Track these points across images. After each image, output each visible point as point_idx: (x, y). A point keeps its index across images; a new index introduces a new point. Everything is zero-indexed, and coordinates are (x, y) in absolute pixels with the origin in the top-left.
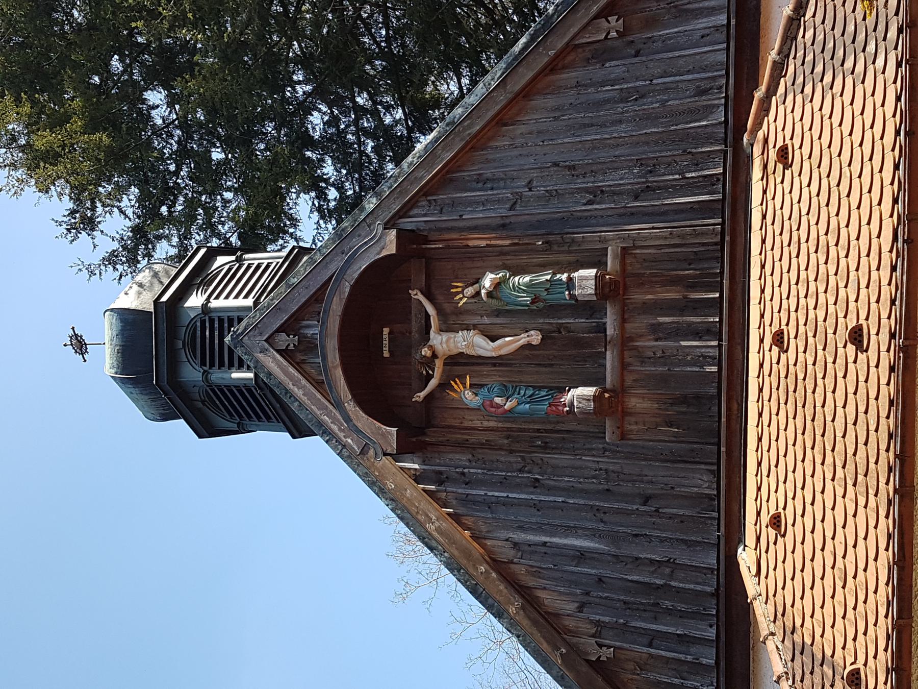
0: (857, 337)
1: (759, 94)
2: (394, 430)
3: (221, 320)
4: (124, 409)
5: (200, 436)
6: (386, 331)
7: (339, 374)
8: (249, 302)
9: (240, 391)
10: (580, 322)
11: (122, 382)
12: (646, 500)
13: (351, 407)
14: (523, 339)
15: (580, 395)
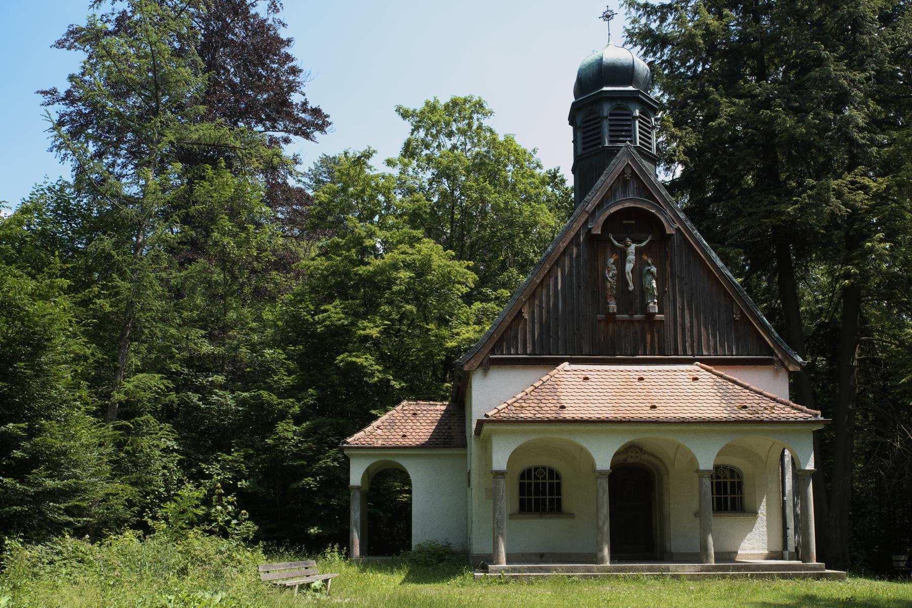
0: (653, 407)
1: (805, 408)
3: (630, 131)
9: (599, 133)
10: (638, 304)
12: (578, 330)
14: (631, 284)
15: (613, 306)
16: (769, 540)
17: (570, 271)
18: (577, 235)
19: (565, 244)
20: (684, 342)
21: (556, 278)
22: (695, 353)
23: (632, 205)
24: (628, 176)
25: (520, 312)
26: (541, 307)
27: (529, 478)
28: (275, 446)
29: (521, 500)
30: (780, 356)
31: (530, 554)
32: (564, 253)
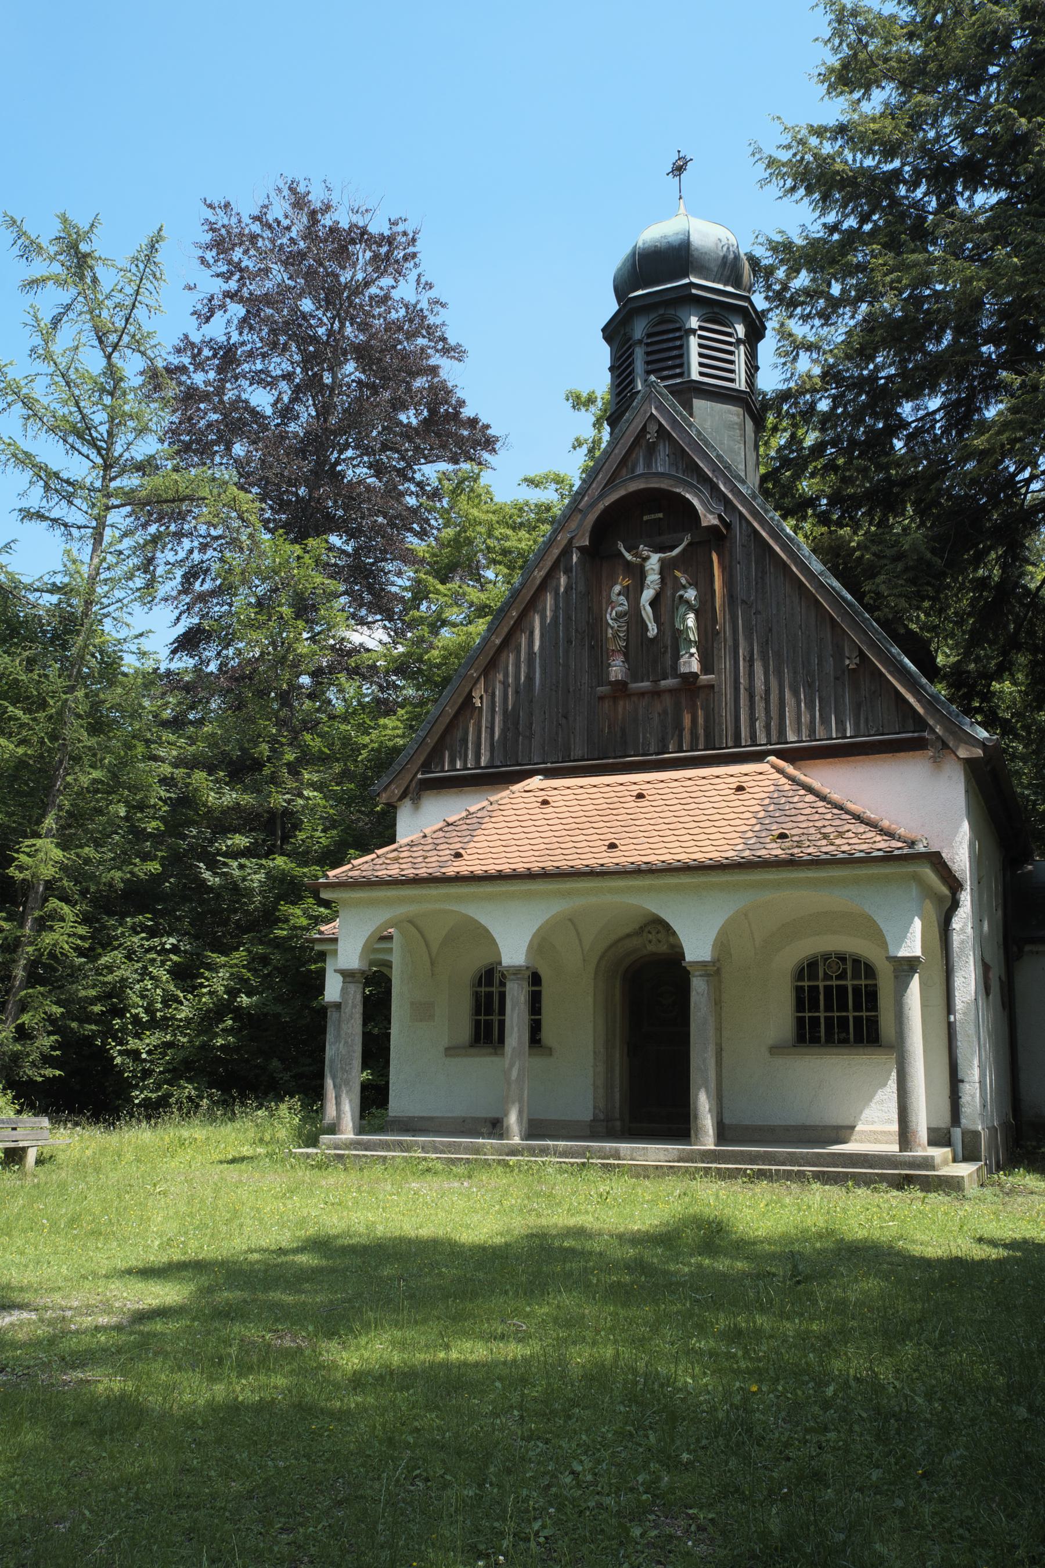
3: (681, 356)
5: (603, 330)
6: (661, 515)
7: (622, 492)
8: (695, 376)
11: (633, 253)
13: (601, 506)
15: (617, 669)
17: (555, 618)
18: (566, 552)
19: (543, 573)
20: (752, 720)
21: (532, 633)
22: (774, 739)
23: (642, 486)
24: (652, 437)
25: (469, 697)
26: (505, 685)
27: (813, 976)
28: (289, 938)
29: (477, 1023)
30: (938, 729)
31: (476, 1120)
32: (543, 587)
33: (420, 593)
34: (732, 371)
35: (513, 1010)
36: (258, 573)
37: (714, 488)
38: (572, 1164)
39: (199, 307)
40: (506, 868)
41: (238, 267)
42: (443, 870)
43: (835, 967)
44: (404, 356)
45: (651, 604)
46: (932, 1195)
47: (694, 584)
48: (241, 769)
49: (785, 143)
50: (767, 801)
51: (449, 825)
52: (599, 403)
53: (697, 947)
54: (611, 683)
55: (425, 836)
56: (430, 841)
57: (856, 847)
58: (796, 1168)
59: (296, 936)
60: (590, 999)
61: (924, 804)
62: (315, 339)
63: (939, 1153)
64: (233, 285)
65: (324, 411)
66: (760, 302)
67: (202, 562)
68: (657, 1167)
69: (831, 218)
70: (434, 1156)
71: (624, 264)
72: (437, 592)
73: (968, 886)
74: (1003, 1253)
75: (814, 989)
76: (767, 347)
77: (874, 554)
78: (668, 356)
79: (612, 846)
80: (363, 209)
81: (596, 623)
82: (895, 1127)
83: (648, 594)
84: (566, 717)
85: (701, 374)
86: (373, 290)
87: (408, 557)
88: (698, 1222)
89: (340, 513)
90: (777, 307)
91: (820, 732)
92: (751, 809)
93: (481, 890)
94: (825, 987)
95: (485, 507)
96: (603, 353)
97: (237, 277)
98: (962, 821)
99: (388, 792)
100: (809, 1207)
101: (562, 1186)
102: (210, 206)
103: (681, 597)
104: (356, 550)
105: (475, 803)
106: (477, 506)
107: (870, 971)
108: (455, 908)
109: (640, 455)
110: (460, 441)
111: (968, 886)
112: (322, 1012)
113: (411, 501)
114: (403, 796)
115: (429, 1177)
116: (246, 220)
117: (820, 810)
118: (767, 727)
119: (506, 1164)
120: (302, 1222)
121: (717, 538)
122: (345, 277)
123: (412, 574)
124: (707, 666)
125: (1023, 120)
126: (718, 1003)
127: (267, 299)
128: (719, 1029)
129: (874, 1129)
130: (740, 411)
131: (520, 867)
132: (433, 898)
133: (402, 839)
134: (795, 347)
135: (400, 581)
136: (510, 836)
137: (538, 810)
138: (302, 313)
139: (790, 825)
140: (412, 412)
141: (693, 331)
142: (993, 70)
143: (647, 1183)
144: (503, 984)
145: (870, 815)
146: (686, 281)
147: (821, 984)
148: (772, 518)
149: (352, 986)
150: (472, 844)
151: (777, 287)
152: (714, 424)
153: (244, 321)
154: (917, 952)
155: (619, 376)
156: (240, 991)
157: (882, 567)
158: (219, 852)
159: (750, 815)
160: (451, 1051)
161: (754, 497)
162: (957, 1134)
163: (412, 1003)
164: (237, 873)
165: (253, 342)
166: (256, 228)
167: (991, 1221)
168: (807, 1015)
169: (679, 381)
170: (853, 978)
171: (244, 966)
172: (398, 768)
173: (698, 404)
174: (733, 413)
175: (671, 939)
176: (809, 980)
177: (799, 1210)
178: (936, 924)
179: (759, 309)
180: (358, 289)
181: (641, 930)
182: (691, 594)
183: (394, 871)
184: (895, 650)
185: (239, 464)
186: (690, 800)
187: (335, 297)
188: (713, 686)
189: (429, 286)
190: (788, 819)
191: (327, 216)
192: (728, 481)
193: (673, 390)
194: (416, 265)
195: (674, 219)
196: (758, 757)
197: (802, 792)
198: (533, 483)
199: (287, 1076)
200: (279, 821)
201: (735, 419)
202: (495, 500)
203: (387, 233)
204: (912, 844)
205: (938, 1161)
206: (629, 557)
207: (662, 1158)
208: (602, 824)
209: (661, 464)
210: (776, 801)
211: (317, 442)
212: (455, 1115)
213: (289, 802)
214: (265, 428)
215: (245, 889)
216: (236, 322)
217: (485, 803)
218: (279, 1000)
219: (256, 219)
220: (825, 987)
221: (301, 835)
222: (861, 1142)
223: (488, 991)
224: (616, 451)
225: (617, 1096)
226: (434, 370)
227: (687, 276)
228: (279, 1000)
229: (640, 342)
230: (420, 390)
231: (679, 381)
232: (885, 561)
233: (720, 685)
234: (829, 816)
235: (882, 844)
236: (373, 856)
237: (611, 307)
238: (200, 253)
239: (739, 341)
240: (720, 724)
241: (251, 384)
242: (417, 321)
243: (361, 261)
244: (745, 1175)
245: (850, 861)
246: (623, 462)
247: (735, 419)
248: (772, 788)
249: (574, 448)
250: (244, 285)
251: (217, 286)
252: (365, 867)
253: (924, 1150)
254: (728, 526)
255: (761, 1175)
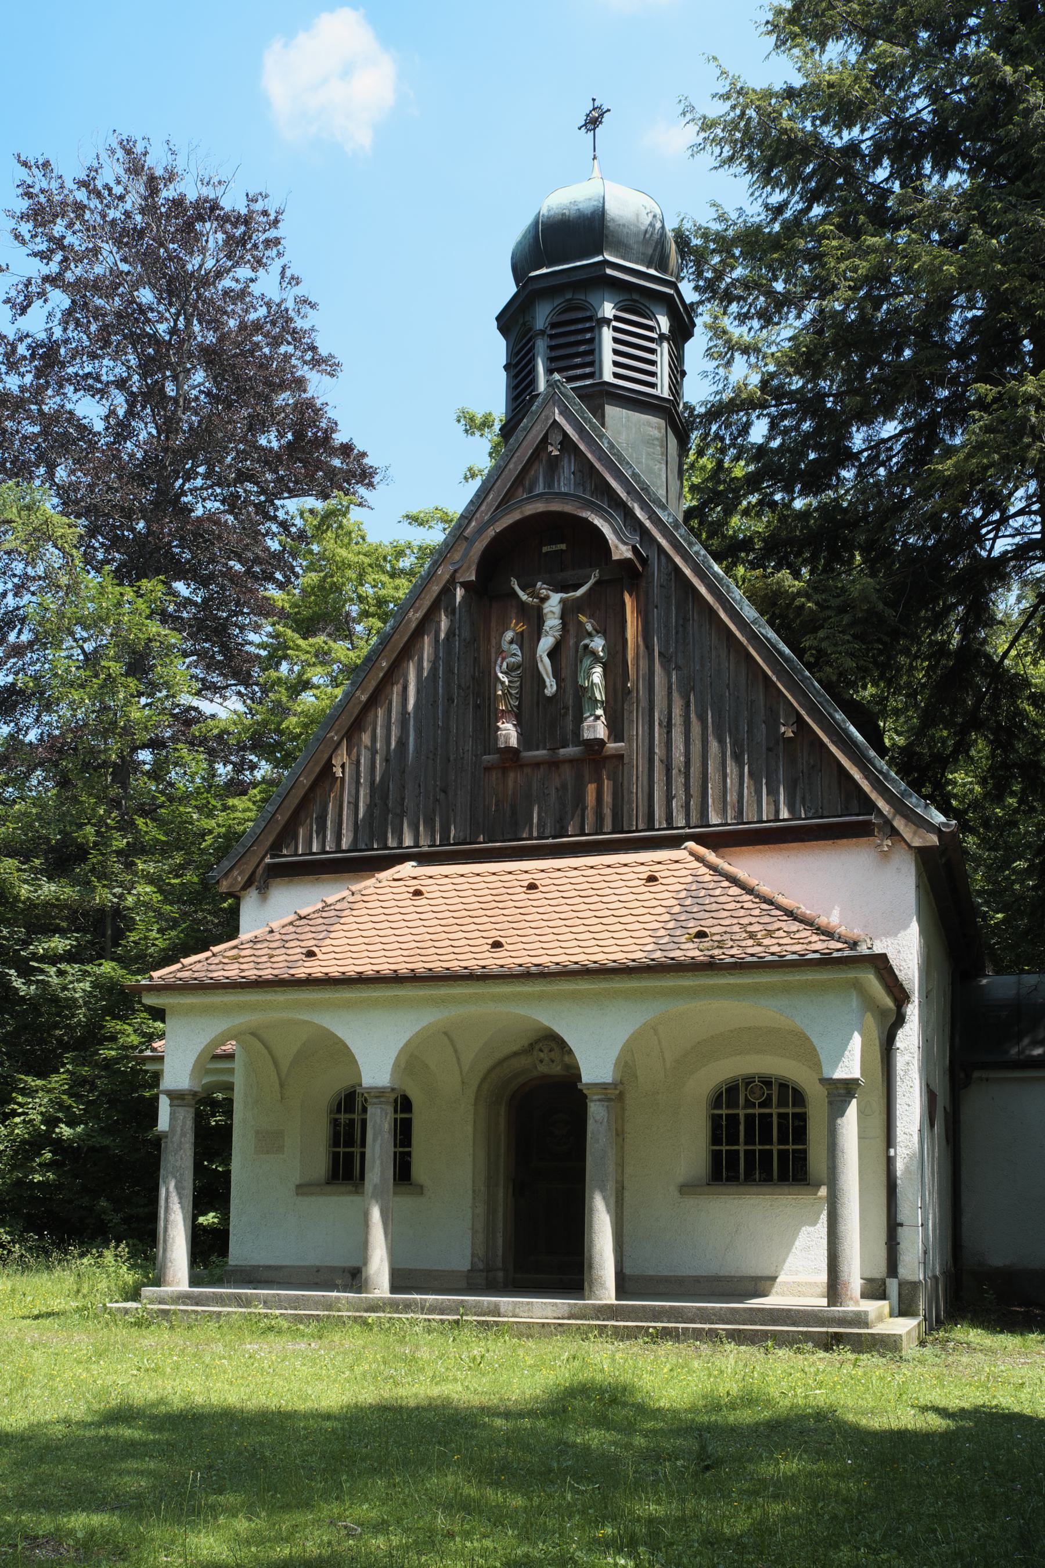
2: (473, 578)
3: (591, 352)
4: (512, 232)
5: (498, 319)
6: (563, 547)
7: (515, 516)
8: (608, 377)
13: (491, 533)
15: (508, 732)
16: (788, 1254)
17: (434, 669)
18: (447, 591)
19: (419, 615)
20: (669, 798)
21: (405, 688)
22: (694, 821)
25: (329, 765)
26: (373, 752)
27: (732, 1103)
28: (116, 1060)
29: (335, 1156)
31: (332, 1269)
33: (278, 653)
34: (653, 374)
35: (374, 1140)
36: (81, 622)
37: (628, 514)
38: (442, 1321)
39: (13, 293)
40: (368, 969)
41: (59, 243)
42: (292, 971)
43: (758, 1093)
44: (263, 365)
45: (549, 655)
46: (865, 1356)
47: (602, 631)
48: (63, 859)
49: (723, 91)
50: (683, 894)
51: (301, 918)
52: (497, 427)
53: (595, 1067)
54: (500, 751)
55: (272, 931)
56: (278, 937)
57: (788, 948)
58: (707, 1326)
59: (126, 1057)
60: (470, 1129)
61: (865, 900)
62: (154, 339)
63: (873, 1307)
64: (54, 268)
65: (168, 427)
66: (688, 292)
67: (18, 608)
68: (543, 1325)
69: (777, 198)
70: (278, 1312)
71: (524, 237)
72: (298, 648)
73: (915, 998)
74: (951, 1424)
75: (733, 1119)
76: (696, 348)
77: (817, 604)
78: (574, 349)
79: (497, 945)
80: (215, 180)
81: (484, 679)
82: (823, 1277)
83: (546, 643)
84: (444, 791)
85: (616, 375)
86: (227, 283)
87: (265, 609)
88: (581, 1391)
89: (187, 555)
90: (709, 300)
91: (749, 814)
92: (664, 903)
93: (338, 995)
94: (747, 1116)
95: (356, 548)
96: (497, 348)
97: (58, 257)
98: (906, 926)
99: (230, 880)
100: (722, 1372)
101: (427, 1349)
102: (25, 164)
103: (586, 646)
104: (205, 601)
105: (334, 893)
106: (347, 546)
107: (799, 1097)
108: (305, 1017)
109: (539, 471)
110: (331, 473)
111: (915, 998)
112: (157, 1142)
113: (274, 545)
114: (248, 885)
115: (271, 1337)
116: (70, 185)
117: (746, 905)
118: (687, 807)
119: (365, 1323)
120: (105, 1391)
121: (631, 575)
122: (193, 263)
123: (270, 629)
124: (616, 730)
125: (1008, 68)
126: (620, 1134)
127: (97, 286)
128: (621, 1165)
129: (798, 1279)
130: (662, 423)
131: (385, 969)
132: (279, 1007)
133: (244, 936)
134: (728, 349)
135: (256, 639)
136: (374, 932)
137: (409, 902)
138: (139, 305)
139: (711, 922)
140: (273, 435)
141: (607, 322)
142: (972, 21)
143: (530, 1343)
144: (365, 1110)
145: (805, 910)
146: (600, 258)
147: (742, 1113)
148: (697, 553)
149: (180, 1109)
150: (328, 942)
151: (709, 275)
152: (631, 437)
153: (69, 313)
154: (856, 1073)
155: (516, 376)
156: (60, 1120)
157: (825, 620)
158: (34, 956)
159: (664, 910)
160: (303, 1189)
161: (677, 526)
162: (893, 1286)
163: (257, 1132)
164: (55, 980)
165: (80, 340)
166: (81, 195)
167: (934, 1387)
168: (724, 1148)
169: (588, 382)
170: (779, 1105)
171: (64, 1092)
172: (242, 850)
173: (612, 412)
174: (652, 425)
175: (566, 1059)
176: (727, 1107)
177: (710, 1375)
178: (877, 1042)
179: (688, 301)
180: (206, 281)
181: (531, 1048)
182: (598, 644)
183: (233, 972)
184: (840, 716)
185: (65, 493)
186: (591, 892)
187: (177, 287)
188: (622, 756)
189: (296, 281)
190: (708, 915)
191: (171, 187)
192: (644, 506)
193: (583, 394)
194: (279, 254)
195: (586, 183)
196: (675, 842)
197: (726, 884)
198: (415, 520)
199: (117, 1218)
200: (109, 920)
201: (656, 433)
202: (369, 539)
203: (244, 211)
204: (854, 945)
205: (872, 1317)
206: (524, 597)
207: (550, 1314)
208: (485, 919)
209: (566, 482)
210: (694, 897)
211: (159, 471)
212: (307, 1264)
213: (121, 897)
214: (92, 445)
215: (67, 999)
216: (59, 315)
217: (346, 893)
218: (107, 1131)
219: (83, 184)
220: (747, 1116)
221: (133, 936)
222: (783, 1294)
223: (347, 1115)
224: (511, 466)
225: (500, 1241)
226: (300, 384)
227: (600, 252)
228: (107, 1131)
229: (542, 332)
230: (282, 409)
231: (588, 382)
232: (829, 613)
233: (630, 756)
234: (757, 912)
235: (820, 945)
236: (208, 954)
237: (508, 289)
238: (12, 223)
239: (662, 337)
240: (630, 802)
241: (76, 391)
242: (282, 325)
243: (211, 244)
244: (647, 1334)
245: (780, 965)
246: (519, 481)
247: (656, 433)
248: (690, 879)
249: (466, 478)
250: (68, 268)
251: (37, 269)
252: (198, 967)
253: (857, 1303)
254: (644, 561)
255: (666, 1334)
